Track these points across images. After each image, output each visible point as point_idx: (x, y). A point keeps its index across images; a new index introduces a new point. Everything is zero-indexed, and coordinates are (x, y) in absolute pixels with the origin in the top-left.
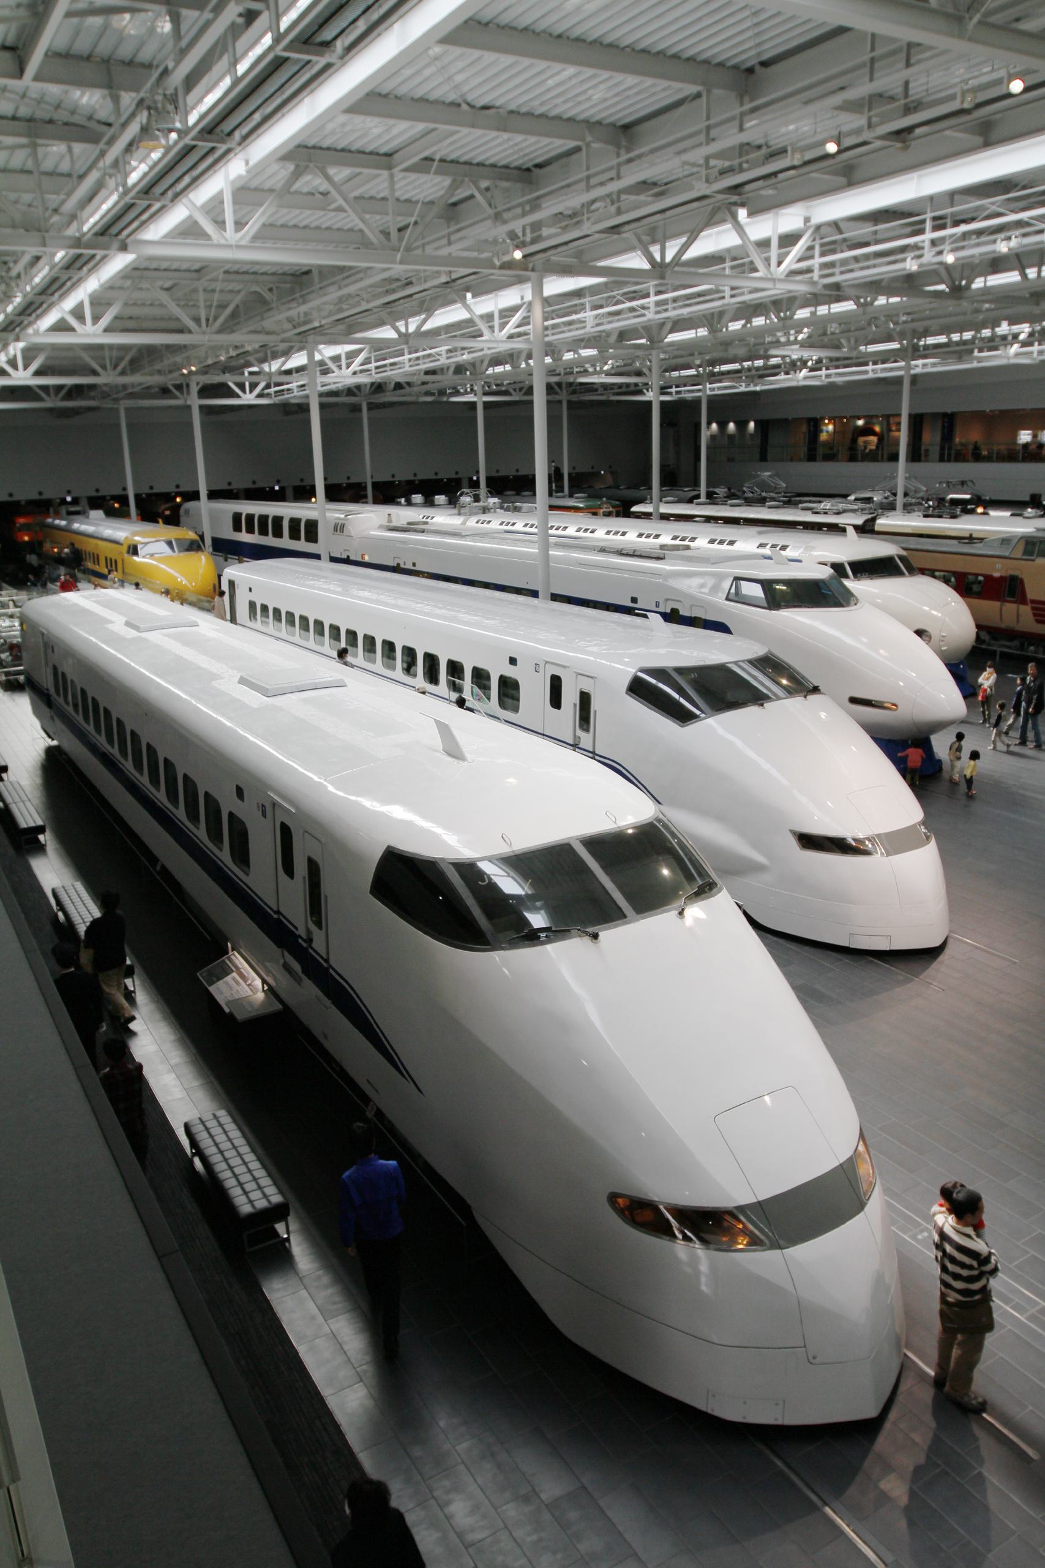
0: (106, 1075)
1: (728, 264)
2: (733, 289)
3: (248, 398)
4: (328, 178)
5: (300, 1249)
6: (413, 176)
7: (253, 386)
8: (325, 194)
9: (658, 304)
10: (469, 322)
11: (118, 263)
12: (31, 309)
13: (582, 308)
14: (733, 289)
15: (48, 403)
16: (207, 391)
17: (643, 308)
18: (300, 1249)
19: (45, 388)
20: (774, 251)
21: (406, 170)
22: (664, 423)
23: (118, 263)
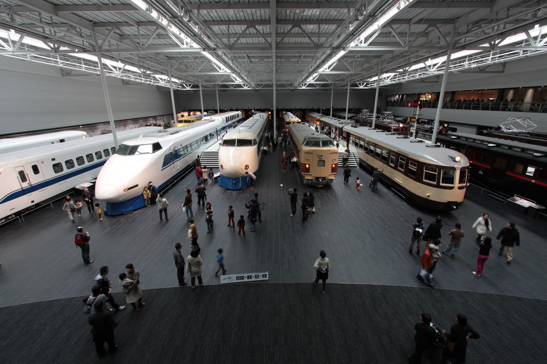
0: (311, 208)
1: (524, 44)
2: (524, 51)
3: (361, 87)
4: (392, 28)
5: (253, 175)
6: (416, 25)
7: (363, 84)
8: (390, 33)
9: (492, 58)
10: (425, 68)
11: (342, 53)
12: (319, 67)
13: (464, 61)
14: (524, 51)
15: (317, 88)
16: (352, 86)
17: (487, 60)
18: (253, 175)
19: (317, 84)
20: (539, 39)
21: (415, 23)
22: (380, 95)
23: (342, 53)
